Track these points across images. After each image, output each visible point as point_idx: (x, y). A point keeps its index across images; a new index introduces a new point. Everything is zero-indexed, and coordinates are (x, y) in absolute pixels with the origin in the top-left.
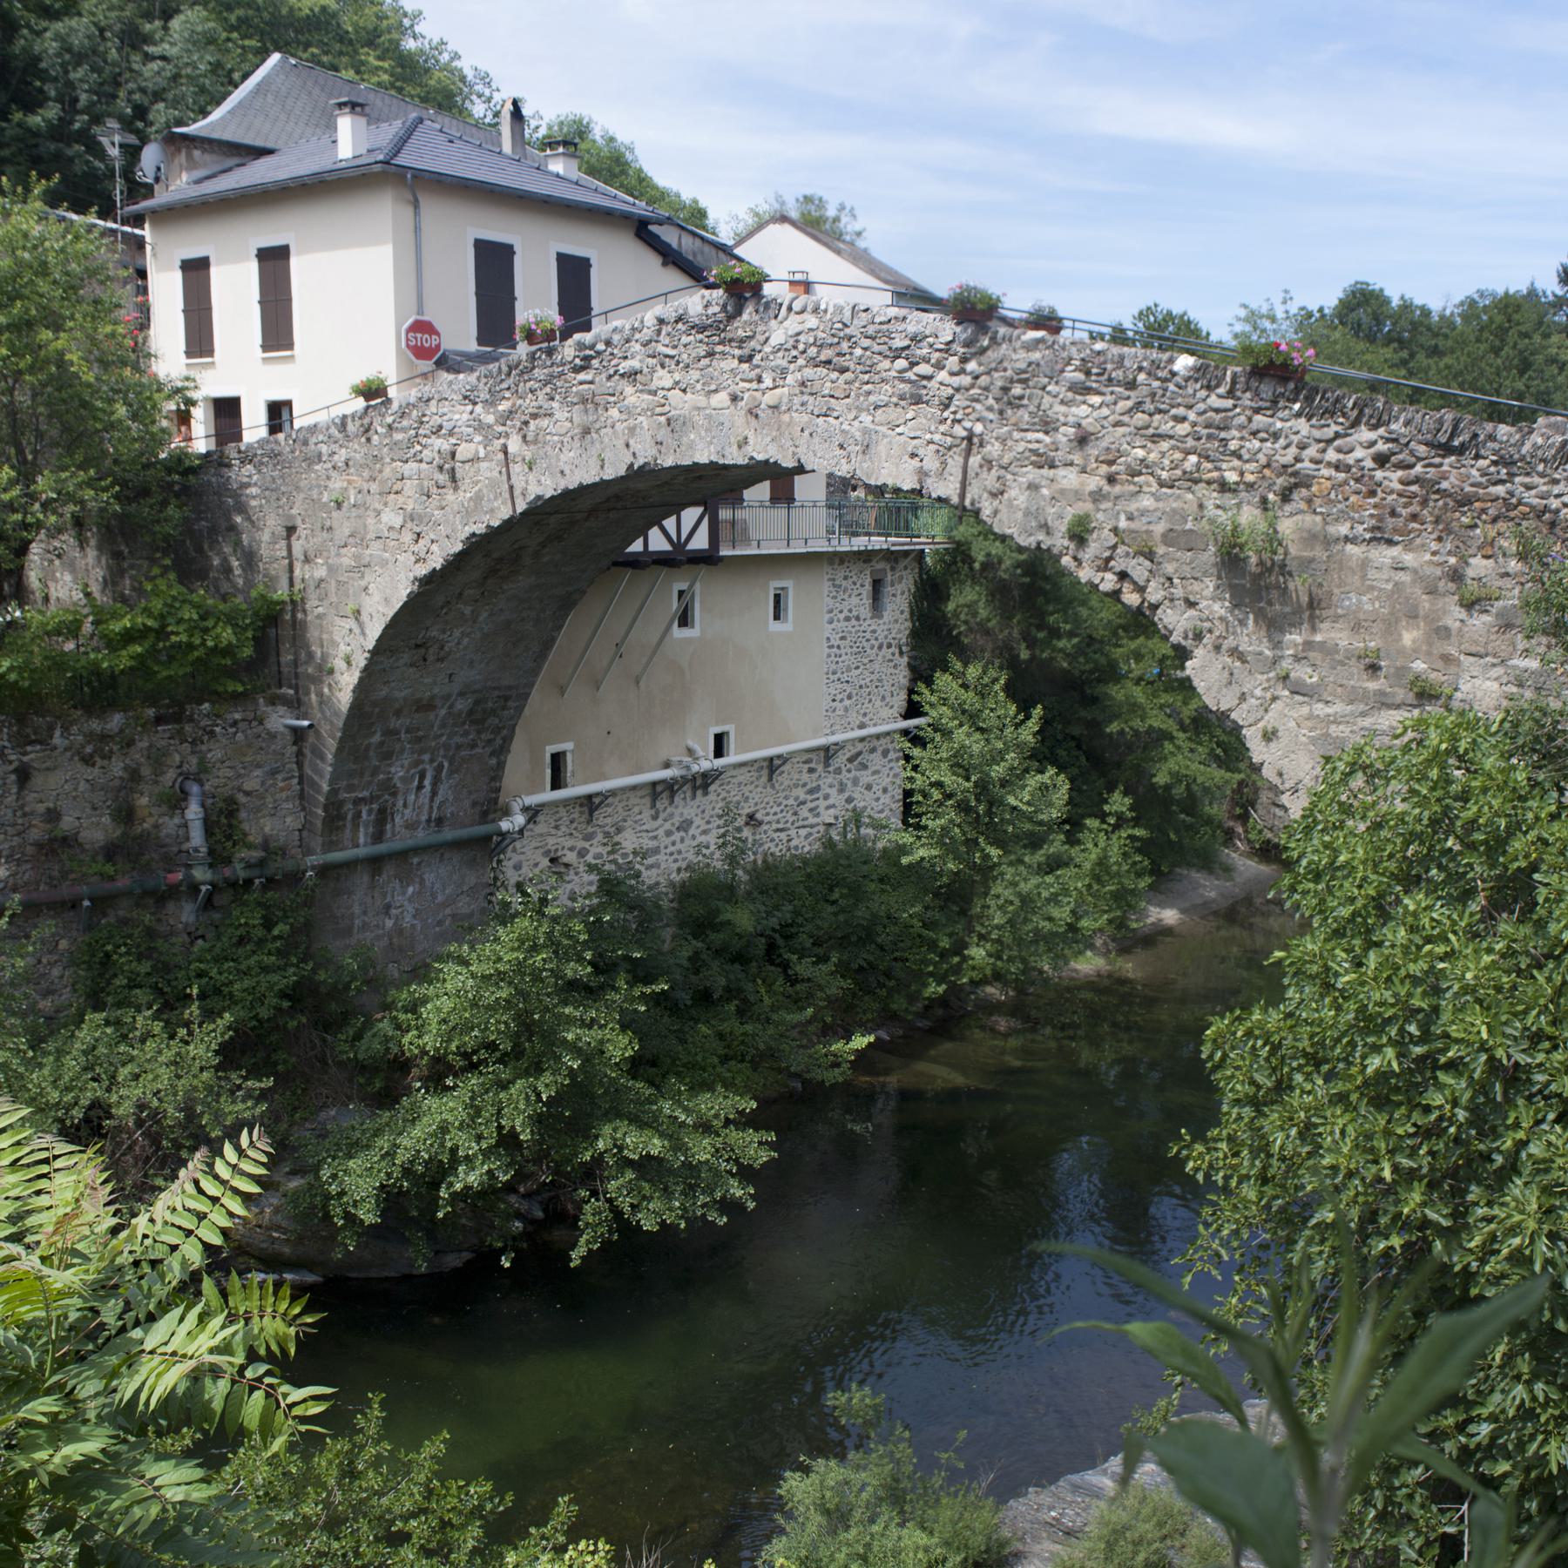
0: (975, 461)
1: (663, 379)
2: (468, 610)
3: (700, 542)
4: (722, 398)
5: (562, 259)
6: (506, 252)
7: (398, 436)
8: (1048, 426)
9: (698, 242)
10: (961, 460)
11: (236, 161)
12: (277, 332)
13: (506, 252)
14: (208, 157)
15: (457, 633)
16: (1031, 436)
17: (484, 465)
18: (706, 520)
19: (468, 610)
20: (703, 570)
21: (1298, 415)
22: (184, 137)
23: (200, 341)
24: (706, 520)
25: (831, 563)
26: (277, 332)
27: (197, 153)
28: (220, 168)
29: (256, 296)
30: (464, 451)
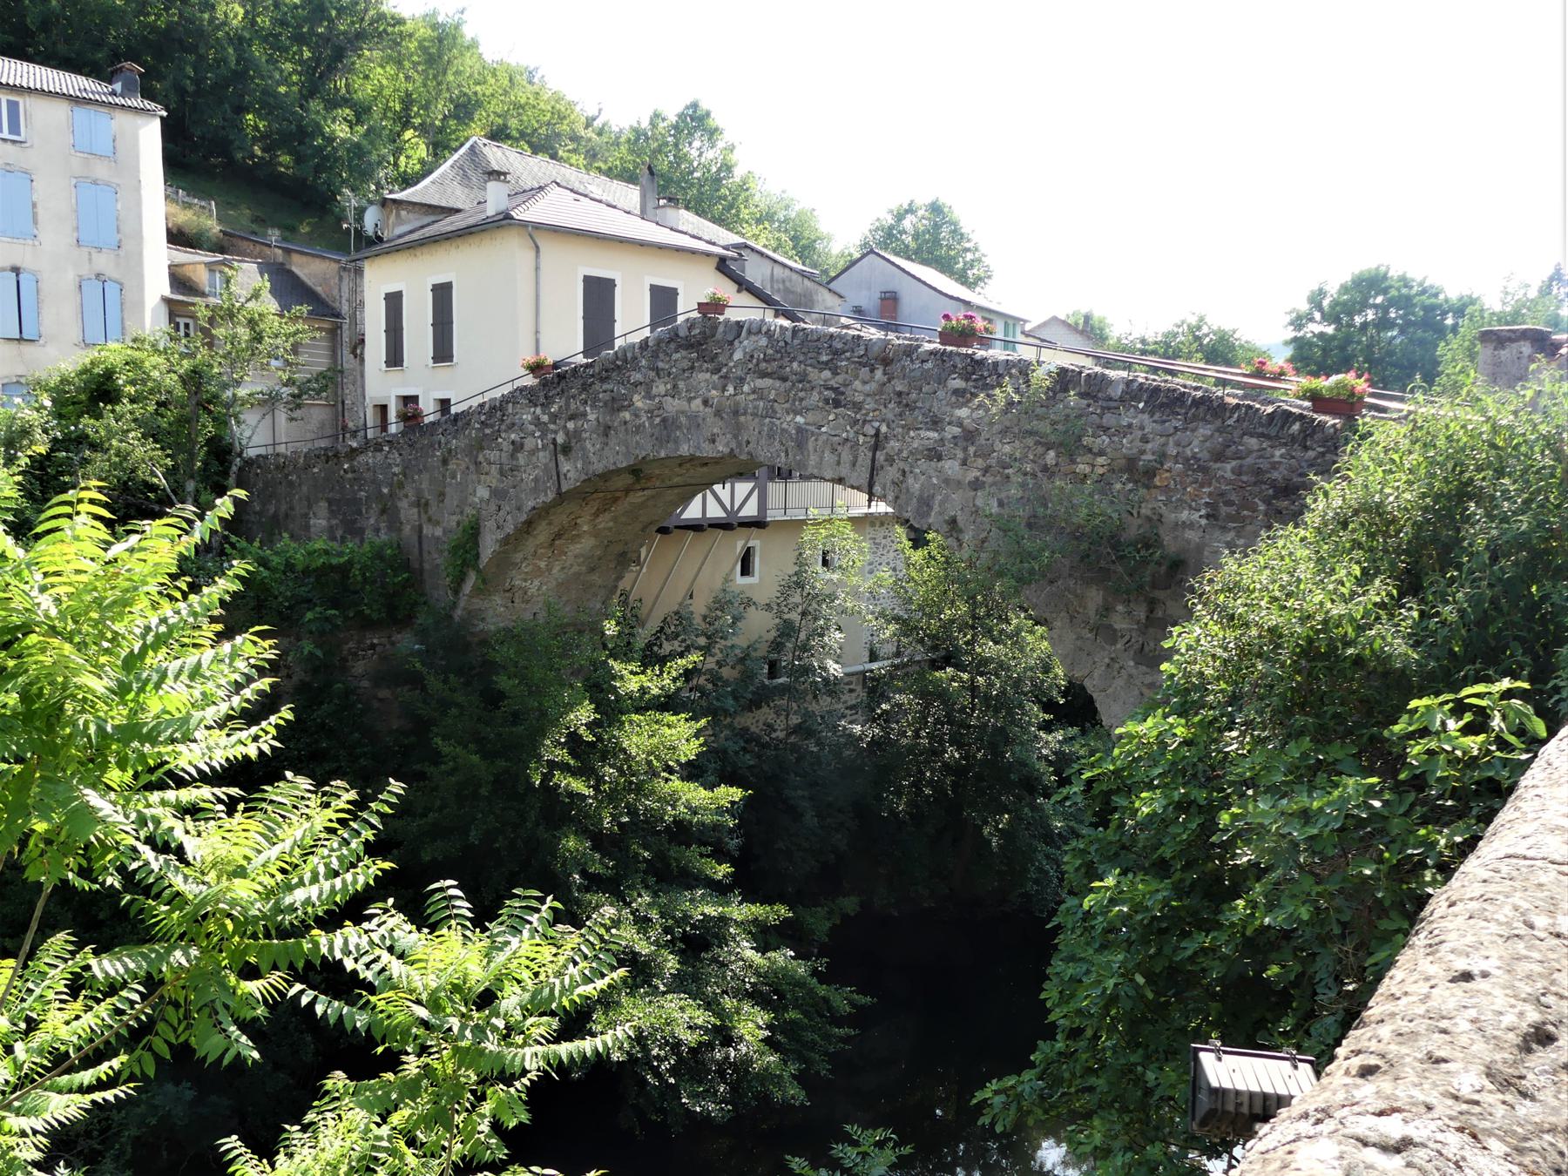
0: (880, 456)
1: (660, 388)
2: (543, 564)
3: (751, 510)
4: (698, 402)
5: (655, 290)
6: (609, 285)
7: (488, 431)
8: (935, 423)
9: (787, 271)
10: (870, 454)
11: (432, 218)
12: (443, 352)
13: (609, 285)
14: (411, 216)
15: (536, 582)
16: (923, 433)
17: (541, 454)
18: (756, 493)
19: (543, 564)
20: (754, 531)
21: (1142, 411)
22: (394, 201)
23: (395, 358)
24: (756, 493)
25: (873, 524)
26: (443, 352)
27: (403, 213)
28: (418, 224)
29: (581, 313)
30: (529, 443)
